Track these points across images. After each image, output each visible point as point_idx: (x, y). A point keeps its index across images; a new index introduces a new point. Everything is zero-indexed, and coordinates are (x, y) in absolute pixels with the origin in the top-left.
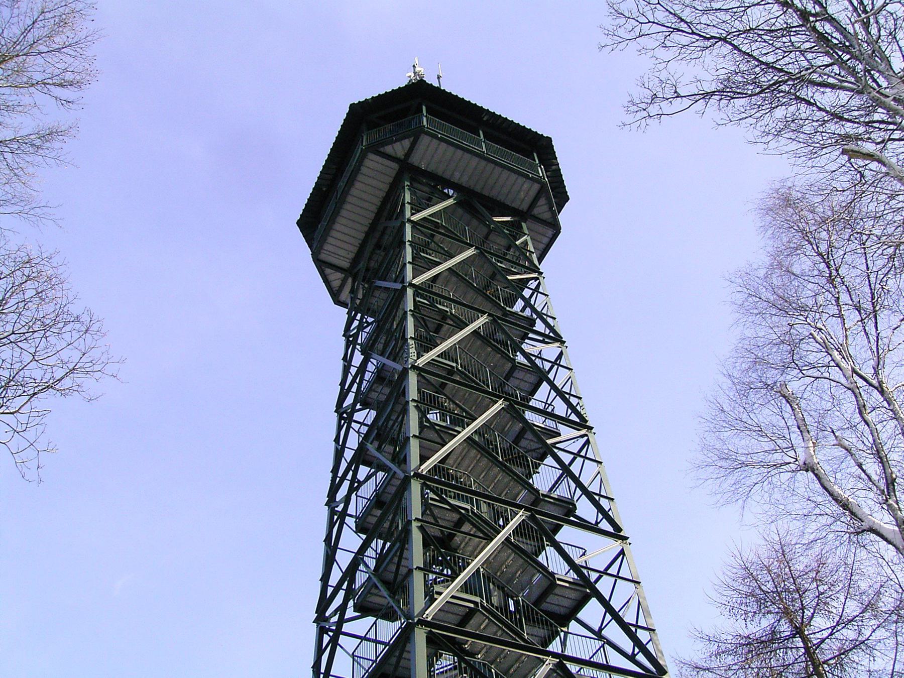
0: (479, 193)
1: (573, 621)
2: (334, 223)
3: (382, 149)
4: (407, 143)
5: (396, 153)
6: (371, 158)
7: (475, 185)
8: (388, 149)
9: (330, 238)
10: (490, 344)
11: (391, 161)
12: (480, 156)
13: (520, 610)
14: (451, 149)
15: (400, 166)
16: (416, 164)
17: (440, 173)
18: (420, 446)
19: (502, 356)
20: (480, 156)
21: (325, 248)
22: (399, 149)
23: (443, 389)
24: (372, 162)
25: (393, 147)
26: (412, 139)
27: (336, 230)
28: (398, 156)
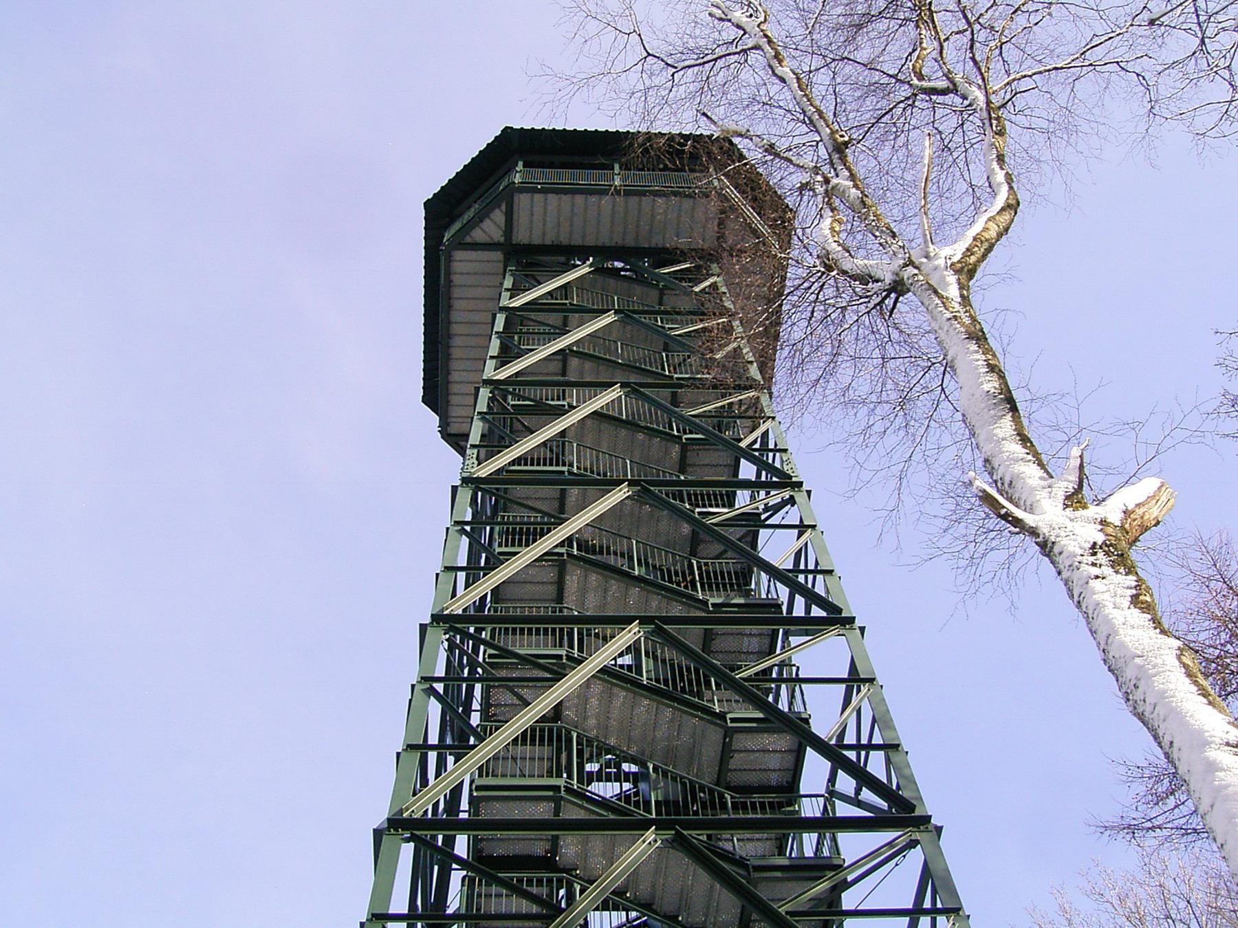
0: (634, 248)
1: (883, 752)
2: (448, 374)
3: (468, 239)
4: (499, 216)
5: (489, 236)
6: (458, 259)
7: (624, 240)
8: (478, 235)
9: (453, 396)
10: (639, 429)
11: (472, 250)
12: (539, 184)
13: (657, 656)
14: (566, 198)
15: (504, 254)
16: (526, 241)
17: (565, 242)
18: (921, 798)
19: (661, 438)
20: (539, 184)
21: (454, 415)
22: (492, 228)
23: (487, 451)
24: (462, 264)
25: (482, 229)
26: (503, 207)
27: (457, 382)
28: (496, 240)
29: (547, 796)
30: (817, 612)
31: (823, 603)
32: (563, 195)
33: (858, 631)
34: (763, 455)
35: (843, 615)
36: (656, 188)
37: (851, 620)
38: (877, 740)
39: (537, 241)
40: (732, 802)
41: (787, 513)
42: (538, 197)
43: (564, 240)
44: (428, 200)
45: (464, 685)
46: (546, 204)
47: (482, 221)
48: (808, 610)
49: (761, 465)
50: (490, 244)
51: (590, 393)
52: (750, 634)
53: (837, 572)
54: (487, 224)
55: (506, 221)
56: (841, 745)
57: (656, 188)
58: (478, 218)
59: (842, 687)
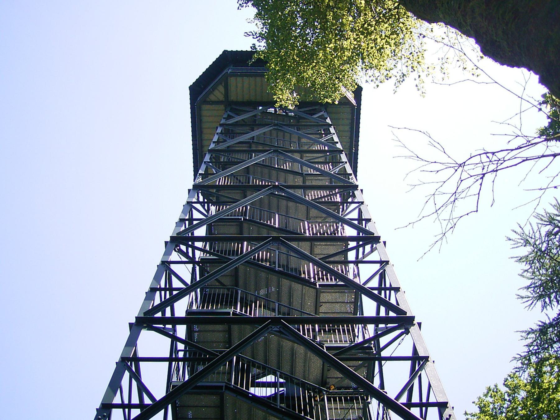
5: (218, 98)
8: (212, 98)
12: (239, 72)
20: (239, 72)
29: (262, 254)
30: (392, 314)
31: (396, 309)
32: (250, 78)
33: (417, 325)
34: (380, 293)
35: (407, 315)
36: (268, 344)
37: (379, 238)
38: (432, 400)
39: (240, 99)
40: (328, 329)
41: (403, 339)
42: (239, 79)
43: (253, 99)
44: (191, 85)
45: (187, 349)
46: (243, 82)
47: (214, 91)
48: (387, 313)
49: (380, 302)
50: (218, 102)
51: (266, 161)
52: (347, 302)
53: (373, 220)
54: (216, 92)
55: (225, 90)
56: (410, 404)
57: (268, 344)
58: (212, 89)
59: (409, 362)
